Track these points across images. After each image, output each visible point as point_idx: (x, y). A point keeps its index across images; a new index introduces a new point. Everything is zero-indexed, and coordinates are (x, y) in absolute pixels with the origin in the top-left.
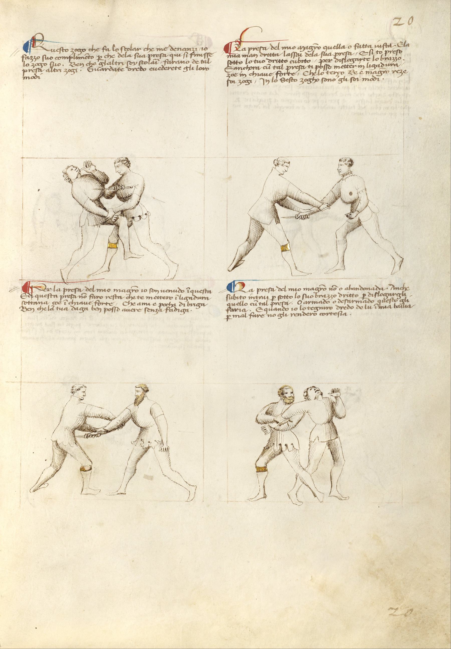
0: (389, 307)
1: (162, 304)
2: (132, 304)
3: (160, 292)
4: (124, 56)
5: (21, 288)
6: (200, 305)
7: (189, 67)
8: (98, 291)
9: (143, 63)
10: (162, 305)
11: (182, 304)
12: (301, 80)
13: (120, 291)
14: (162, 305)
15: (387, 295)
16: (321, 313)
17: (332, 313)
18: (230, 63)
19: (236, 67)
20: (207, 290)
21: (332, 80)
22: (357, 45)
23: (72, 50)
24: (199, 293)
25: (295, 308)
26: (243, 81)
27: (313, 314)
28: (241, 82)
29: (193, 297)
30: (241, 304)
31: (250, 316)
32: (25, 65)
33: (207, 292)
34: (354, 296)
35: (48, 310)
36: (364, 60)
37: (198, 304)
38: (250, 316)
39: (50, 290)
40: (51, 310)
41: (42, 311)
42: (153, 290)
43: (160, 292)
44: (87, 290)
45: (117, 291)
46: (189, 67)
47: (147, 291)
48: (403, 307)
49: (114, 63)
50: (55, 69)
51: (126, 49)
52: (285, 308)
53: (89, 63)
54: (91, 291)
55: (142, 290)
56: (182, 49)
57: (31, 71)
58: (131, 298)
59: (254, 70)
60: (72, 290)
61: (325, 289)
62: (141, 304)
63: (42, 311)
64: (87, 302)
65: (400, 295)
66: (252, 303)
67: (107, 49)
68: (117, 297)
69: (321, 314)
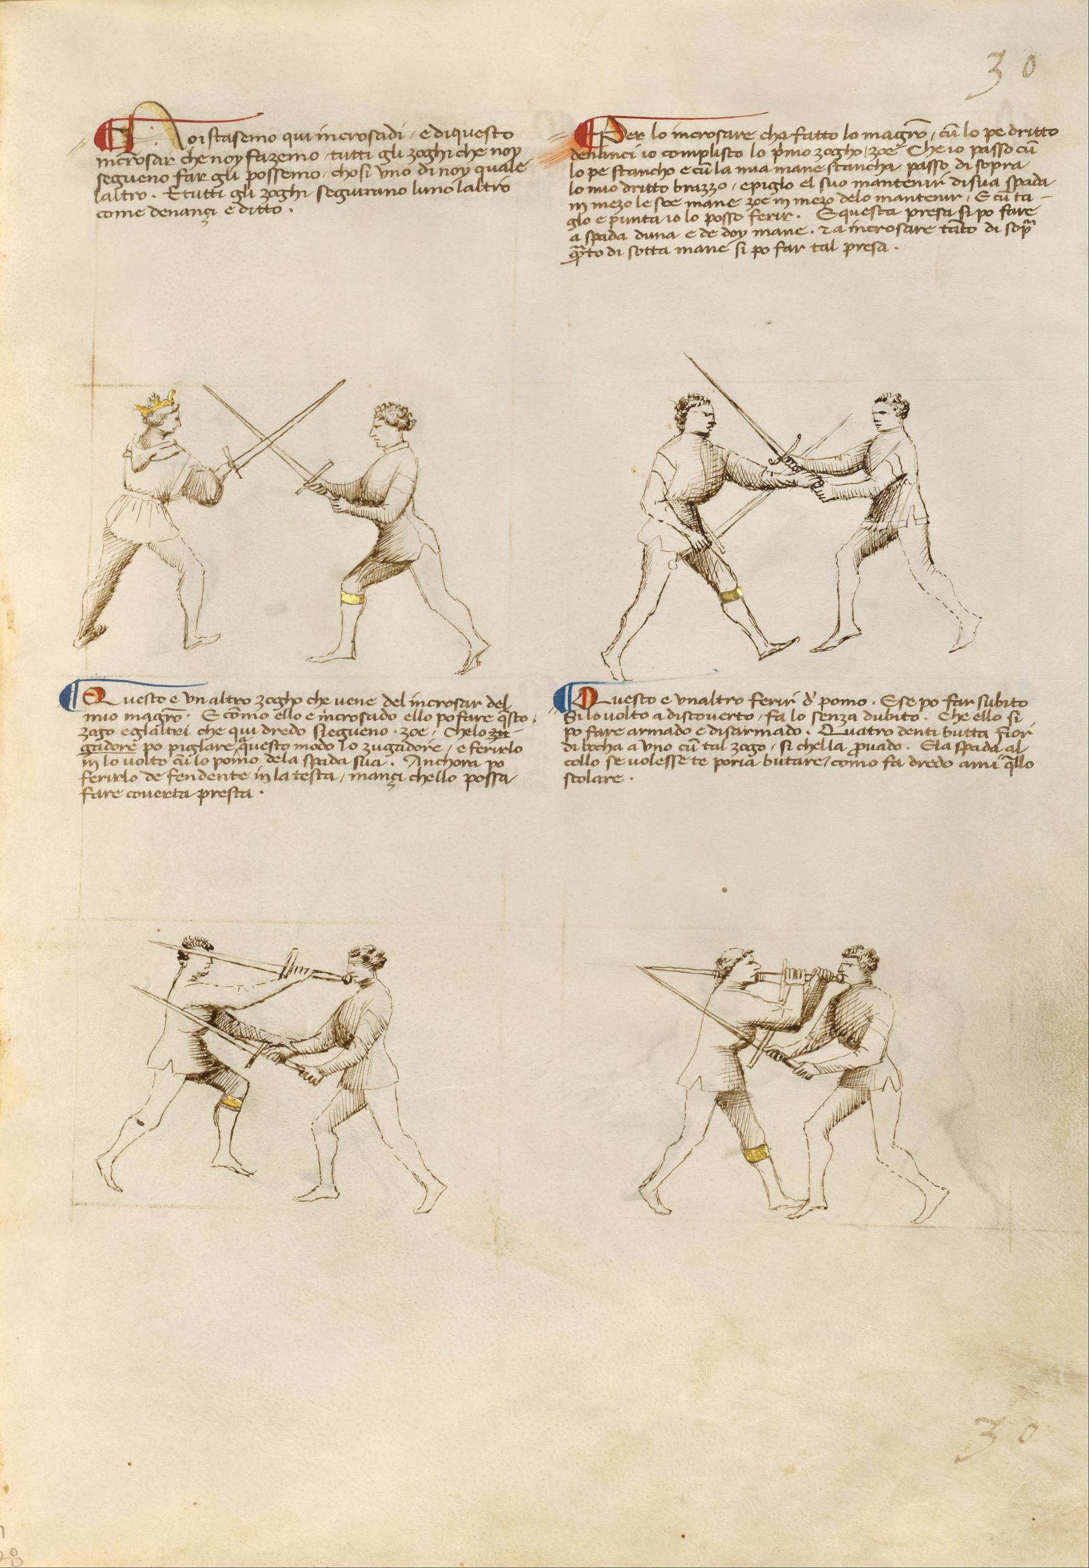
0: (838, 747)
1: (496, 762)
2: (960, 718)
3: (792, 203)
4: (412, 718)
5: (92, 141)
6: (906, 136)
7: (780, 182)
8: (213, 162)
9: (576, 780)
10: (494, 764)
11: (959, 181)
12: (260, 698)
13: (176, 215)
14: (494, 764)
15: (756, 748)
16: (569, 761)
17: (363, 153)
18: (1005, 151)
19: (635, 730)
20: (322, 772)
21: (693, 250)
22: (254, 153)
23: (365, 746)
24: (609, 208)
25: (578, 172)
26: (741, 747)
27: (482, 719)
28: (408, 732)
29: (406, 746)
30: (585, 761)
31: (753, 254)
32: (689, 218)
33: (239, 794)
34: (741, 717)
35: (588, 782)
36: (739, 719)
37: (774, 183)
38: (753, 254)
39: (171, 162)
40: (290, 762)
41: (882, 171)
42: (328, 189)
43: (792, 203)
44: (844, 200)
45: (258, 139)
46: (391, 150)
47: (284, 136)
48: (420, 719)
49: (225, 700)
50: (169, 730)
51: (576, 777)
52: (793, 729)
53: (912, 216)
54: (397, 706)
55: (337, 700)
56: (308, 156)
57: (610, 780)
58: (810, 747)
59: (783, 175)
60: (222, 794)
61: (506, 189)
62: (191, 213)
63: (882, 171)
64: (636, 761)
65: (283, 193)
66: (477, 168)
67: (466, 717)
68: (698, 762)
69: (569, 763)
